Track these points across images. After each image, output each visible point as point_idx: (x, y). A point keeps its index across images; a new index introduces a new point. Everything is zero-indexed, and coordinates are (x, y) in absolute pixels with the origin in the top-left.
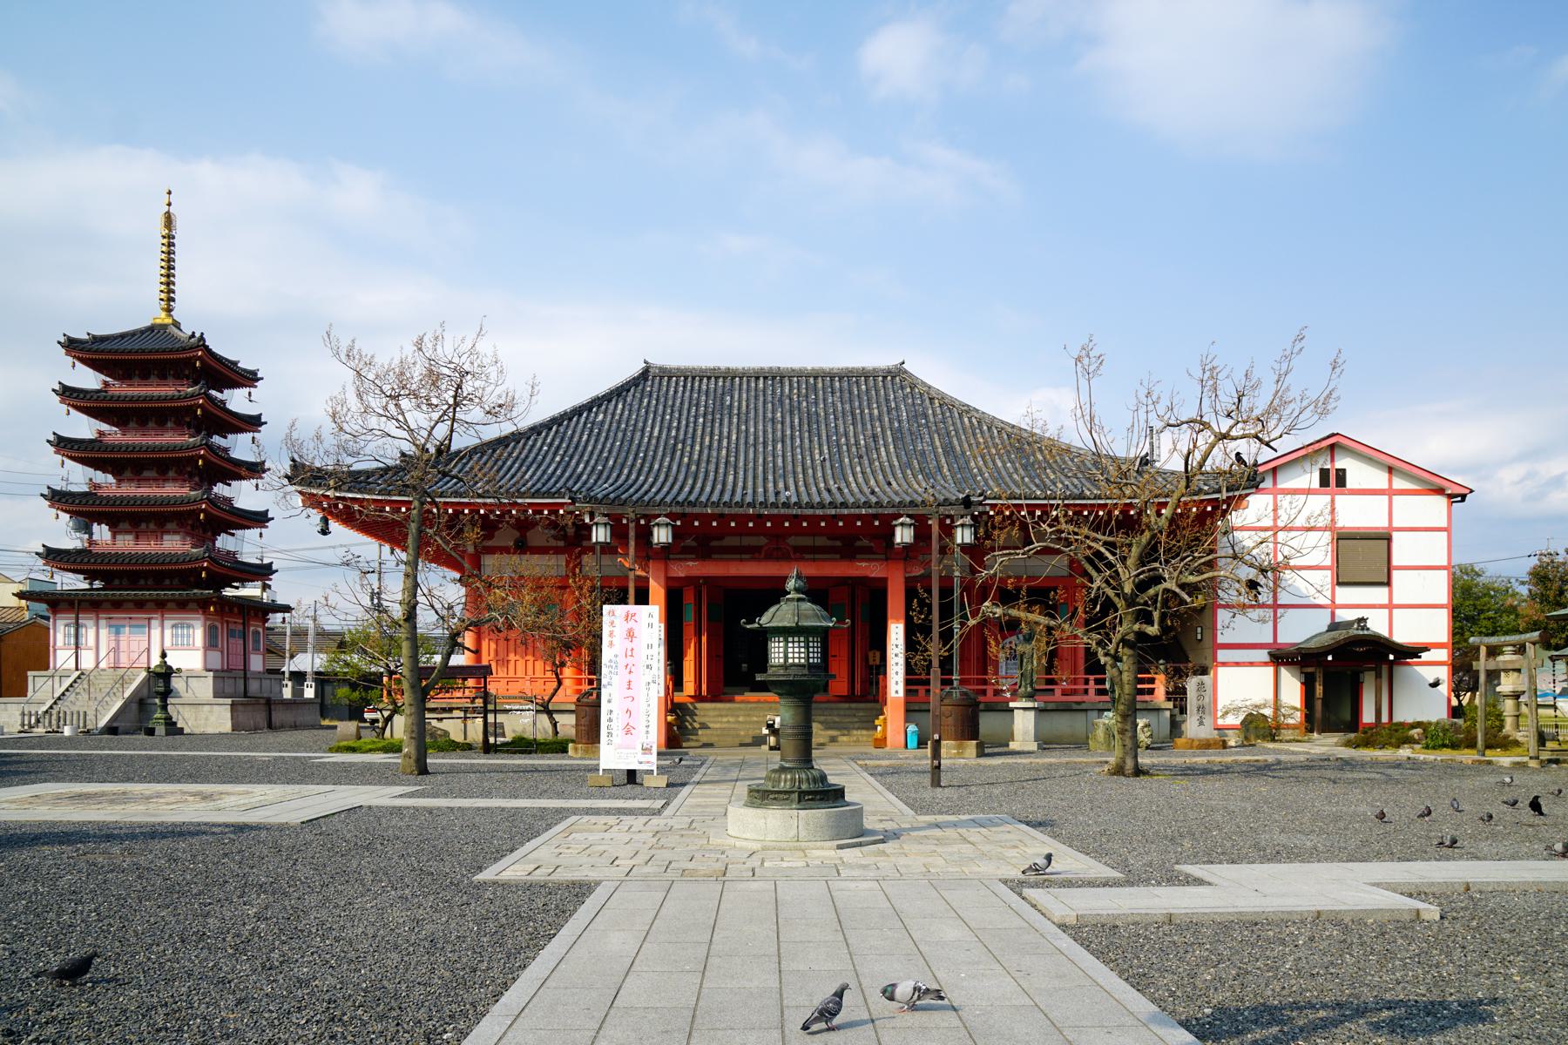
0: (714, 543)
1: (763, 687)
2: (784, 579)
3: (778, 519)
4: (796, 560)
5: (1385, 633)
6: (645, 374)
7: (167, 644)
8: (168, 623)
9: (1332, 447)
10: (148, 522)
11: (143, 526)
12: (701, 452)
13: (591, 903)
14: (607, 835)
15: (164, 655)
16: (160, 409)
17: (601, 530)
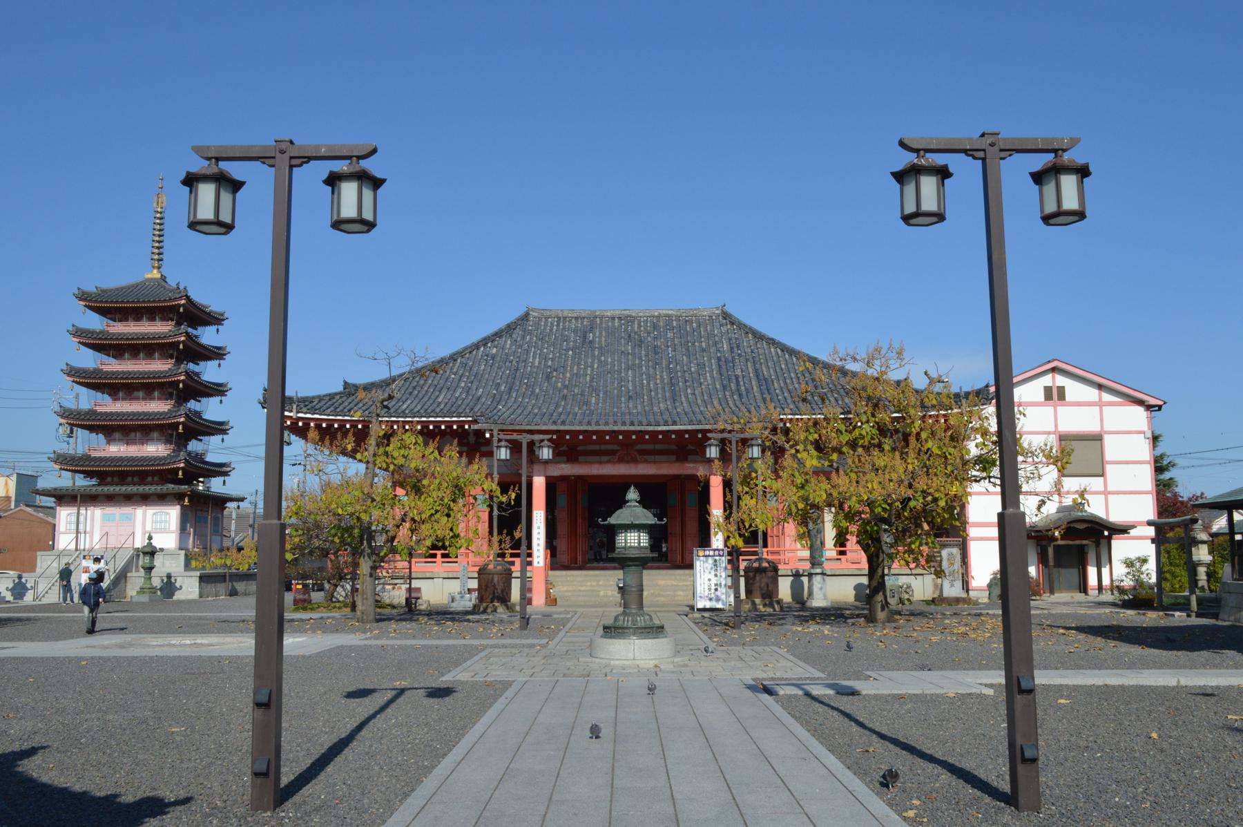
1: (613, 560)
6: (527, 315)
13: (509, 693)
16: (151, 359)
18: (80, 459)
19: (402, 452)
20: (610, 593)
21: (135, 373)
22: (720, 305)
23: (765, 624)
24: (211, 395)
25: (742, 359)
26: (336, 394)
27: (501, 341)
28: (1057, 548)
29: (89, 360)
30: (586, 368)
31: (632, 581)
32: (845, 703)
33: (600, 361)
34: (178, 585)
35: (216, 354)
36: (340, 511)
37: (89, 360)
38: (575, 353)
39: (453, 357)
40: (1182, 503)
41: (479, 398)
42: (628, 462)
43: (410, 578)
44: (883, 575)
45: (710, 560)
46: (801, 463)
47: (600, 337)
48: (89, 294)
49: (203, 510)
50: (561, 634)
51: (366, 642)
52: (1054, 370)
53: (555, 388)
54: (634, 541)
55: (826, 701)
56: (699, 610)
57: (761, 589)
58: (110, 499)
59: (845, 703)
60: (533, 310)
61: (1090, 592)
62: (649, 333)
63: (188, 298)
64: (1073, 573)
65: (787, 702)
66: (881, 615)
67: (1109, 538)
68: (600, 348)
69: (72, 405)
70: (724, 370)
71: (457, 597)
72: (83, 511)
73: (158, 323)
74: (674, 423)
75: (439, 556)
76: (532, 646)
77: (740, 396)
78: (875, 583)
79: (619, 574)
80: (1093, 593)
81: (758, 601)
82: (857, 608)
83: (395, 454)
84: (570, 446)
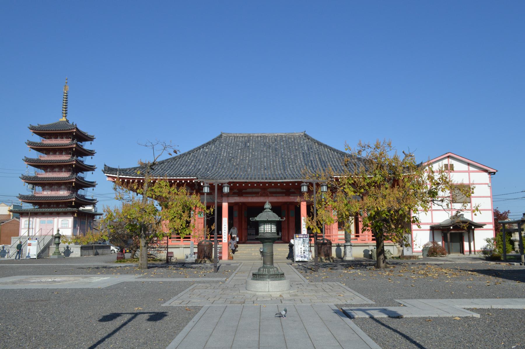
0: (244, 191)
1: (257, 239)
2: (264, 203)
5: (471, 220)
6: (221, 136)
14: (206, 290)
15: (58, 231)
16: (63, 154)
17: (206, 188)
18: (31, 197)
19: (159, 189)
20: (257, 254)
21: (54, 160)
22: (303, 131)
23: (328, 269)
24: (88, 171)
25: (313, 153)
26: (137, 168)
27: (210, 146)
28: (451, 234)
29: (35, 155)
30: (246, 157)
31: (267, 250)
32: (394, 323)
33: (252, 154)
34: (71, 251)
35: (90, 153)
36: (129, 217)
37: (35, 155)
38: (241, 151)
39: (189, 153)
40: (501, 215)
41: (200, 169)
42: (264, 196)
43: (167, 248)
44: (383, 246)
45: (302, 239)
46: (346, 194)
47: (252, 145)
48: (35, 127)
49: (84, 219)
50: (234, 274)
51: (137, 280)
52: (448, 157)
53: (233, 165)
54: (268, 229)
55: (382, 321)
56: (296, 262)
57: (324, 252)
58: (43, 214)
59: (394, 323)
60: (224, 133)
61: (465, 253)
62: (273, 143)
63: (77, 128)
64: (457, 245)
65: (360, 323)
66: (382, 265)
67: (473, 230)
68: (252, 149)
69: (26, 174)
70: (305, 158)
71: (189, 256)
72: (31, 219)
73: (65, 140)
74: (285, 178)
76: (218, 282)
77: (313, 168)
78: (379, 250)
79: (261, 246)
80: (467, 253)
81: (323, 258)
82: (367, 261)
83: (156, 190)
84: (238, 189)
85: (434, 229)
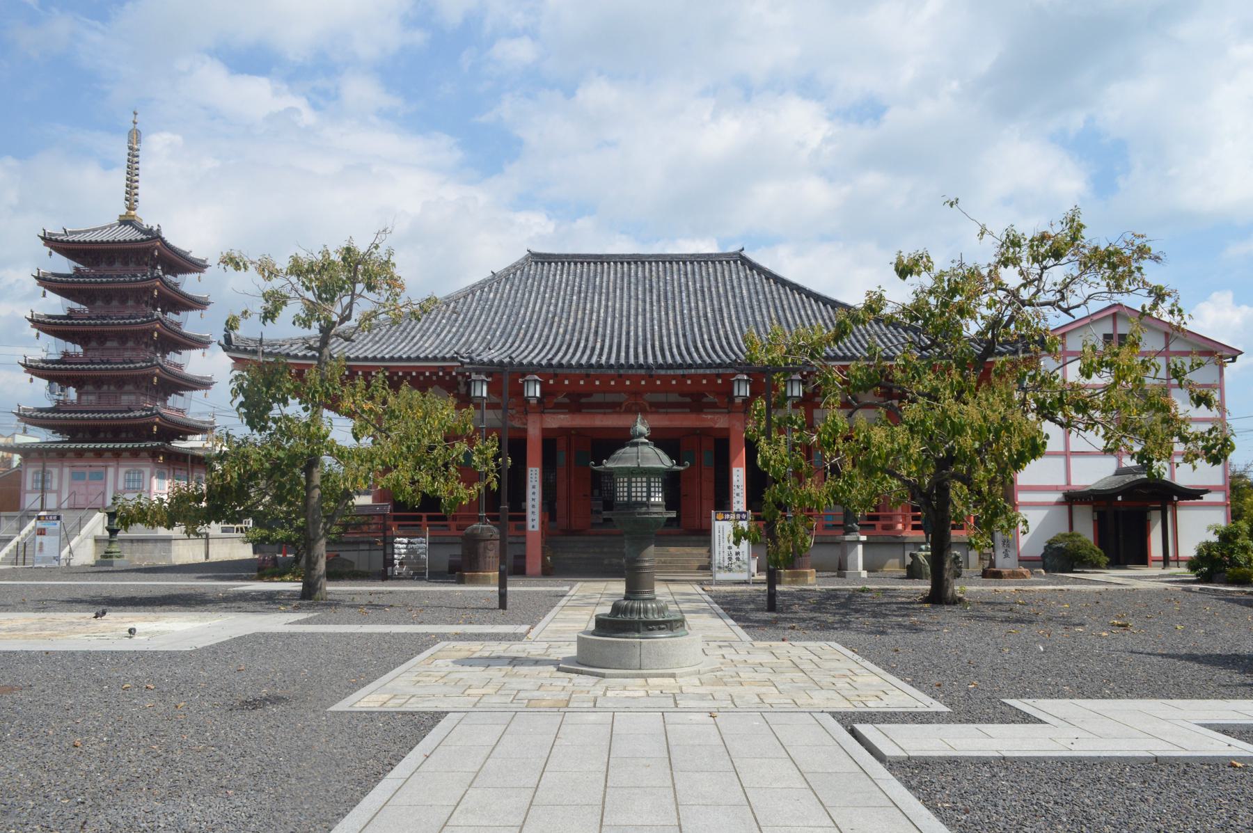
0: (583, 400)
3: (636, 379)
4: (652, 413)
7: (121, 486)
8: (122, 471)
9: (1114, 315)
10: (109, 385)
11: (105, 387)
12: (575, 324)
13: (444, 724)
24: (193, 347)
75: (424, 520)
85: (1073, 499)
